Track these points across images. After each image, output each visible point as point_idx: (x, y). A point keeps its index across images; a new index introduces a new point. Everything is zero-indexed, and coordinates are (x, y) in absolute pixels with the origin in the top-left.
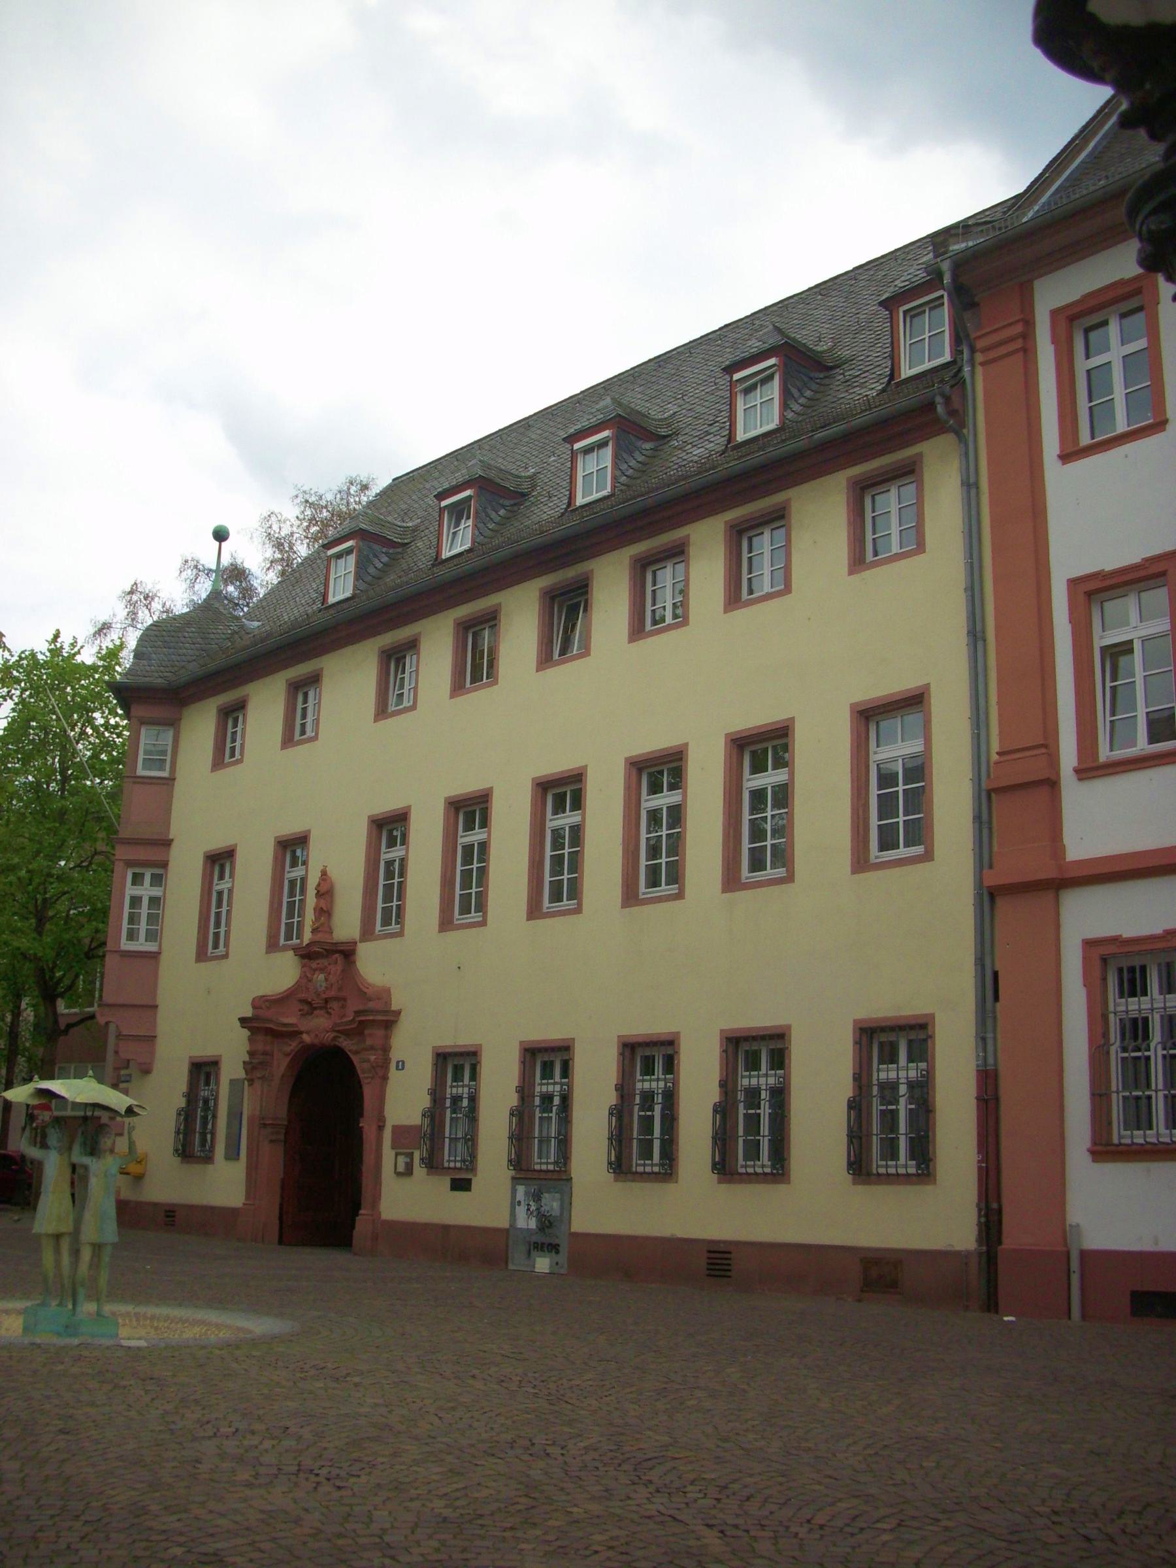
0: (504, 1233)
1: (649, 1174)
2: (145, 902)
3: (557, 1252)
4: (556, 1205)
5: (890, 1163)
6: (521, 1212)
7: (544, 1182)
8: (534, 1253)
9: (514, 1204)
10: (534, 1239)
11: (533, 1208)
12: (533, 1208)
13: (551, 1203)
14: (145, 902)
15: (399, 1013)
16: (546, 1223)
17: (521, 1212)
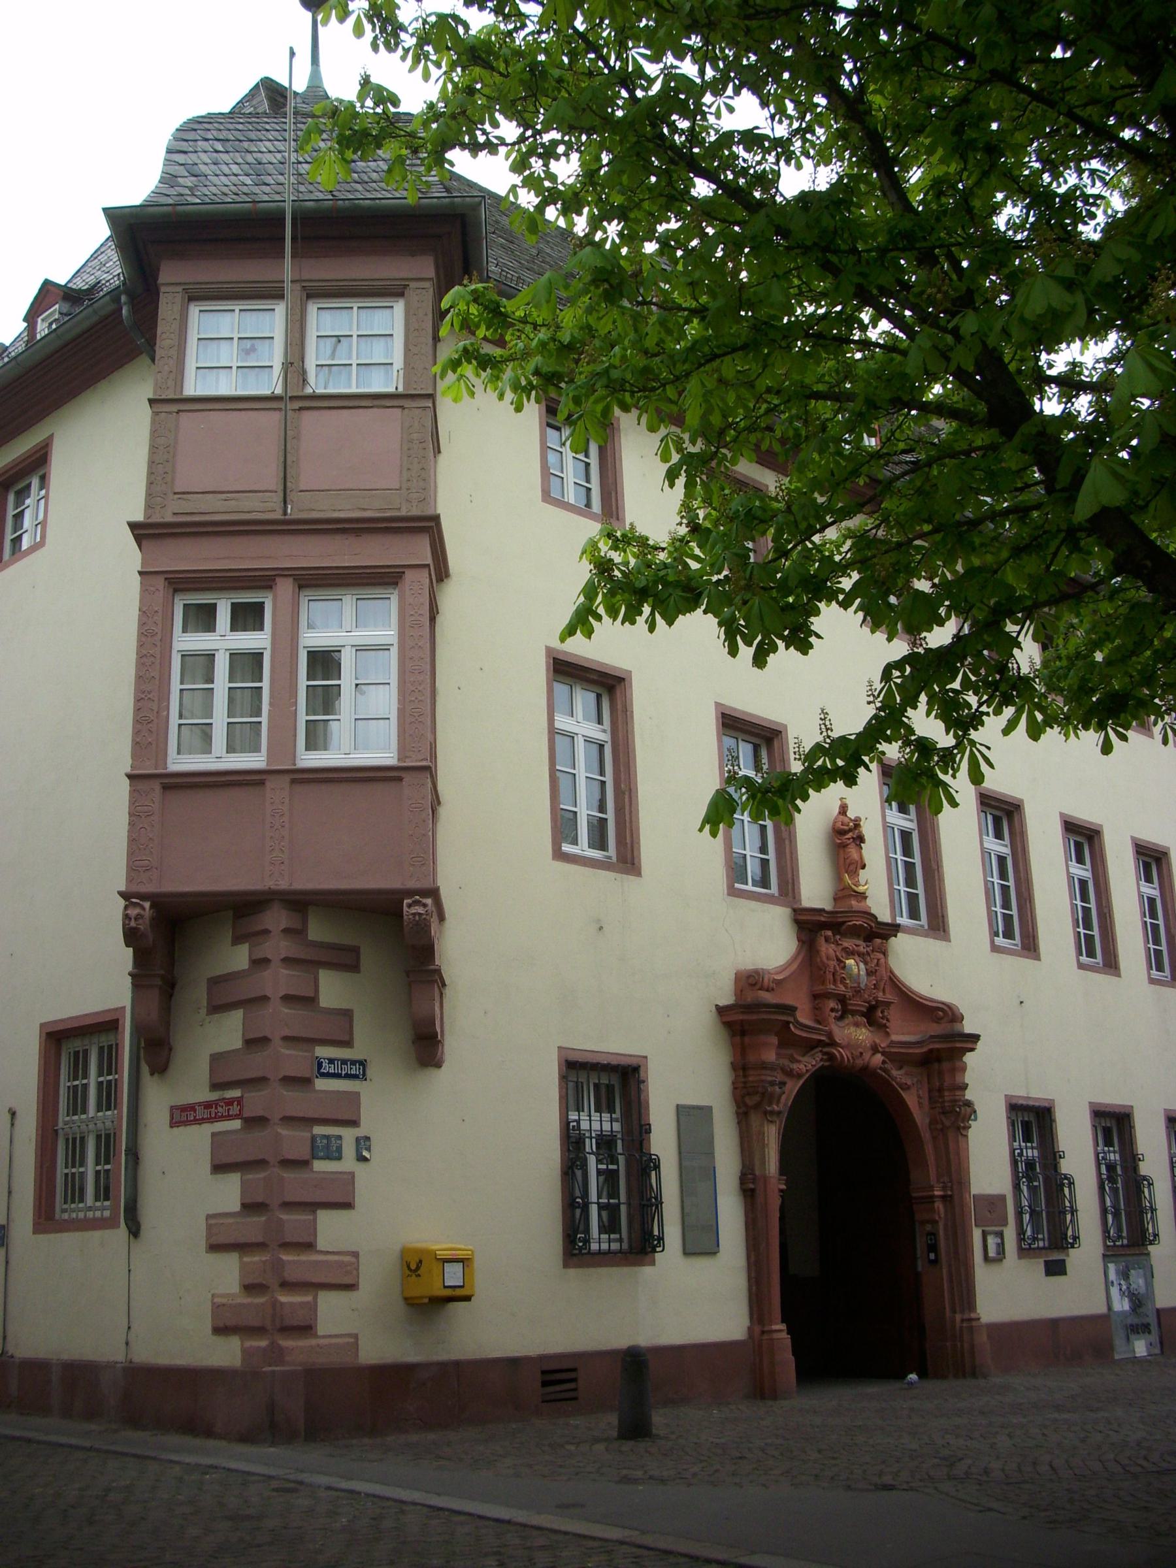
0: (1102, 1321)
1: (615, 1253)
2: (222, 666)
3: (1149, 1332)
4: (1141, 1282)
5: (612, 1236)
6: (1114, 1291)
7: (1130, 1258)
8: (1132, 1337)
9: (1108, 1284)
10: (1129, 1321)
11: (1124, 1287)
12: (1124, 1287)
13: (1138, 1281)
14: (222, 666)
15: (975, 1038)
16: (1138, 1301)
17: (1114, 1291)
